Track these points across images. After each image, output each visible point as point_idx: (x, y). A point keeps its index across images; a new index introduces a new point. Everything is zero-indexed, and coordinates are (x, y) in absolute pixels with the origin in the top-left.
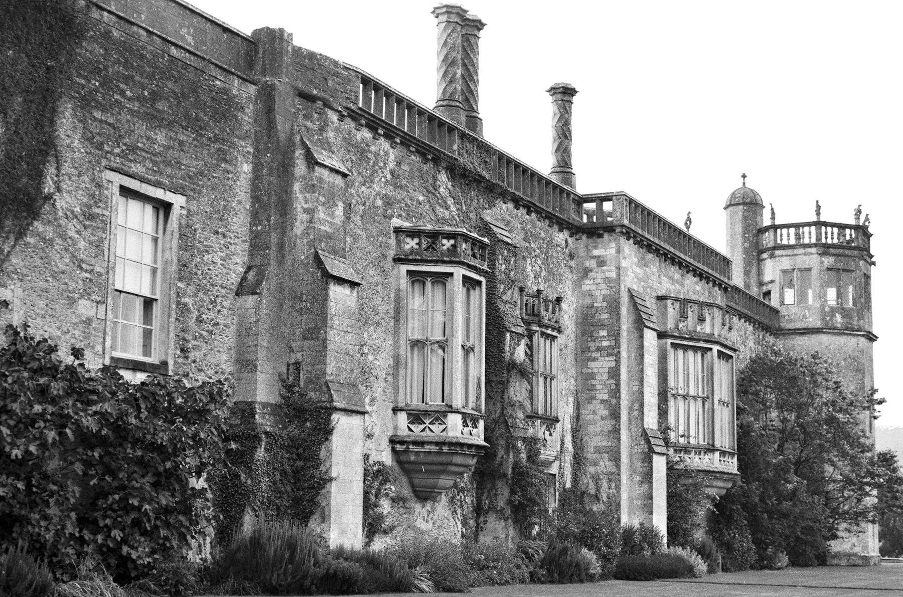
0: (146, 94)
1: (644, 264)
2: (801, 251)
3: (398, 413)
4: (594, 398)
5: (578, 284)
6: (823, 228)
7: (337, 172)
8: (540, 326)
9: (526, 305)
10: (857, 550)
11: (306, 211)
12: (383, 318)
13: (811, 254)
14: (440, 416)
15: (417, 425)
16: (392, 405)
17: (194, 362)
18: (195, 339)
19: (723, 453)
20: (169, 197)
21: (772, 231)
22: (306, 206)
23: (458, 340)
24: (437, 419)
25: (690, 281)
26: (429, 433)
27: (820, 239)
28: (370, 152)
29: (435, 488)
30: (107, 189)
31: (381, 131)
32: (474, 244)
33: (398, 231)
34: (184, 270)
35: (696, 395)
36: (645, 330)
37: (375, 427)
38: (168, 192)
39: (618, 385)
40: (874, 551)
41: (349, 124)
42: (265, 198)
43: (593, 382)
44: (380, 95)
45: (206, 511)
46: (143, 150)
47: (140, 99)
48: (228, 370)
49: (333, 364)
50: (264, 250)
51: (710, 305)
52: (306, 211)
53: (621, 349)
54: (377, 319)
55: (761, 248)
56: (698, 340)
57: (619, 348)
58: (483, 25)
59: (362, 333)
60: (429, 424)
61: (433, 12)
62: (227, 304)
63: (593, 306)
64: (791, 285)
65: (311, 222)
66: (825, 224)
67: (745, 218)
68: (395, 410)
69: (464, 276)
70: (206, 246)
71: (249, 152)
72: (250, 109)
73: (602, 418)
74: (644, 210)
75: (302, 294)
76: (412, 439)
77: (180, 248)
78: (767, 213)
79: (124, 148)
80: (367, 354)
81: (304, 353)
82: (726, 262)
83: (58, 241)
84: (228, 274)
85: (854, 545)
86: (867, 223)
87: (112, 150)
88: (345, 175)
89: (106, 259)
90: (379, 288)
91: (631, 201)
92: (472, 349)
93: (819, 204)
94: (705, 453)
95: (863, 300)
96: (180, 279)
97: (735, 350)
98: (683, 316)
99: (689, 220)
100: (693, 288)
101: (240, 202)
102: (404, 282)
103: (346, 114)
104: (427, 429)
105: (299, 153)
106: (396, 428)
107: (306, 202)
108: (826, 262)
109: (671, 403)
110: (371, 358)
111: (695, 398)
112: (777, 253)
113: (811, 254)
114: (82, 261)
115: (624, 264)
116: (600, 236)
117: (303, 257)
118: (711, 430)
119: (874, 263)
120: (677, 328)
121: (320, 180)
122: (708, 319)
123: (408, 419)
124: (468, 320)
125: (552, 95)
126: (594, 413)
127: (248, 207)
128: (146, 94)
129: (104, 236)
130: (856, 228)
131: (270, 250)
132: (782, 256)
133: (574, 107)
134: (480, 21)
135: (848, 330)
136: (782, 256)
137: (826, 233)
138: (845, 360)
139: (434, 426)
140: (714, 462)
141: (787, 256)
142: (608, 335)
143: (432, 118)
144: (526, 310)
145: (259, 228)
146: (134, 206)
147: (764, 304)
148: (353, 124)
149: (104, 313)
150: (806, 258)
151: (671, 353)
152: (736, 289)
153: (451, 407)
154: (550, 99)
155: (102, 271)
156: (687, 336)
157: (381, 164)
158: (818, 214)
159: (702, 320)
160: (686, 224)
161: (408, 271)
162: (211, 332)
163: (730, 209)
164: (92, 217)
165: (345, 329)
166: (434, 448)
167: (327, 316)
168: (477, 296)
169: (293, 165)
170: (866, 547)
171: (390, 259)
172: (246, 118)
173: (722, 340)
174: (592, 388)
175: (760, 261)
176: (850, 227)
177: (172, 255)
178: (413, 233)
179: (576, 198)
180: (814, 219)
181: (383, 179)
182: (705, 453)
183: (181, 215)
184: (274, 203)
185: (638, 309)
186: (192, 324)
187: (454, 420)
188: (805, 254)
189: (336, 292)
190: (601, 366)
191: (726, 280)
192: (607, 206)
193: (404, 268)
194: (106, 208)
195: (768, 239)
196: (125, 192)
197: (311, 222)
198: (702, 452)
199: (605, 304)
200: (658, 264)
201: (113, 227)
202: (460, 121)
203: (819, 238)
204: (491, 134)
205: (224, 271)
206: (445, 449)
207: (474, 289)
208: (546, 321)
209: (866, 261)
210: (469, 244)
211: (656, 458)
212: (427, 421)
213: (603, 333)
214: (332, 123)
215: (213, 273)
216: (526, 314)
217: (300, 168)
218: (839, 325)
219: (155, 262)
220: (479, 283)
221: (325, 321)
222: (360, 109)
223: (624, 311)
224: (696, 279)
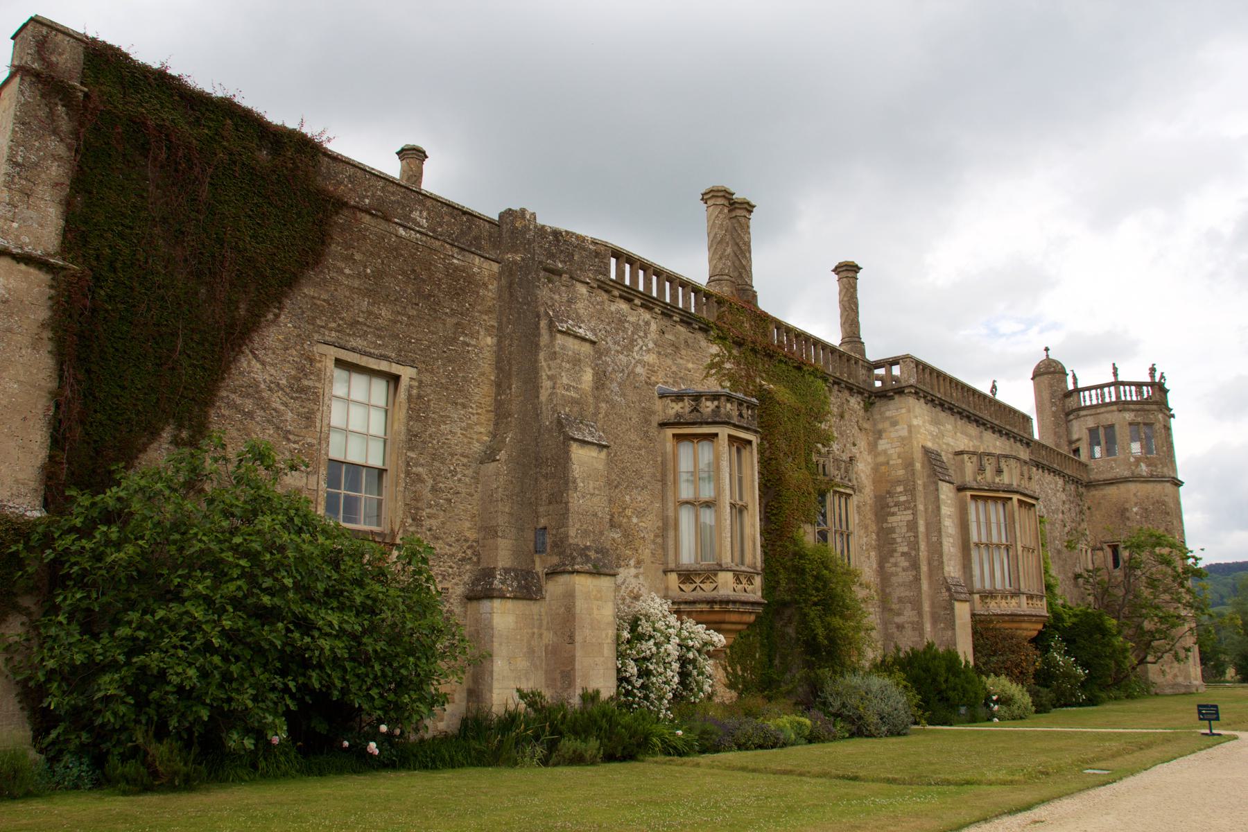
0: (369, 271)
1: (936, 422)
2: (1103, 410)
4: (895, 551)
5: (873, 447)
6: (1122, 388)
7: (583, 339)
10: (1180, 680)
13: (1113, 411)
14: (710, 574)
15: (688, 584)
16: (662, 567)
17: (430, 530)
18: (430, 506)
20: (395, 369)
22: (549, 373)
24: (708, 578)
25: (989, 436)
28: (628, 322)
30: (320, 361)
31: (637, 301)
32: (740, 404)
33: (662, 396)
34: (413, 439)
37: (642, 589)
38: (394, 364)
39: (916, 537)
40: (1196, 679)
43: (894, 536)
44: (634, 267)
45: (251, 691)
46: (365, 324)
47: (361, 276)
48: (472, 538)
49: (577, 526)
51: (1006, 457)
52: (550, 378)
56: (998, 491)
61: (702, 199)
62: (469, 472)
64: (1098, 444)
65: (554, 388)
66: (1124, 384)
67: (1051, 386)
69: (729, 436)
70: (442, 416)
71: (493, 326)
72: (493, 286)
73: (904, 570)
74: (932, 371)
77: (410, 418)
78: (1070, 380)
79: (341, 322)
82: (1026, 419)
83: (260, 413)
84: (470, 443)
85: (1175, 676)
87: (327, 324)
88: (593, 343)
89: (318, 430)
90: (643, 452)
92: (746, 507)
94: (1012, 597)
96: (411, 449)
99: (994, 388)
100: (994, 444)
101: (483, 374)
102: (669, 445)
107: (550, 369)
109: (974, 554)
110: (635, 520)
111: (998, 546)
112: (1082, 413)
113: (1113, 411)
114: (289, 432)
116: (891, 398)
119: (1173, 416)
120: (975, 480)
121: (563, 348)
122: (1005, 469)
123: (679, 578)
124: (740, 480)
126: (896, 565)
127: (493, 378)
128: (369, 271)
129: (316, 407)
130: (1152, 384)
132: (1086, 416)
134: (857, 266)
136: (1086, 416)
138: (1153, 504)
140: (1021, 606)
146: (359, 381)
147: (1076, 461)
149: (315, 483)
151: (972, 507)
153: (721, 565)
154: (836, 277)
155: (314, 442)
157: (642, 334)
158: (1115, 374)
159: (999, 471)
160: (992, 391)
162: (449, 501)
163: (1037, 379)
164: (303, 390)
165: (592, 491)
166: (705, 607)
169: (539, 335)
170: (1187, 677)
171: (655, 424)
172: (490, 294)
173: (1021, 490)
174: (893, 541)
176: (1146, 384)
177: (400, 426)
178: (679, 397)
180: (1112, 379)
183: (411, 387)
186: (427, 494)
187: (726, 579)
188: (1108, 412)
189: (577, 452)
191: (1026, 435)
192: (896, 370)
193: (670, 432)
194: (319, 380)
195: (1071, 403)
196: (339, 363)
197: (554, 388)
199: (900, 461)
201: (326, 399)
202: (725, 290)
203: (1118, 397)
205: (466, 440)
206: (717, 607)
210: (736, 405)
211: (957, 605)
212: (698, 581)
213: (900, 489)
215: (454, 441)
217: (545, 338)
218: (1145, 474)
219: (385, 434)
221: (567, 483)
222: (612, 280)
223: (918, 466)
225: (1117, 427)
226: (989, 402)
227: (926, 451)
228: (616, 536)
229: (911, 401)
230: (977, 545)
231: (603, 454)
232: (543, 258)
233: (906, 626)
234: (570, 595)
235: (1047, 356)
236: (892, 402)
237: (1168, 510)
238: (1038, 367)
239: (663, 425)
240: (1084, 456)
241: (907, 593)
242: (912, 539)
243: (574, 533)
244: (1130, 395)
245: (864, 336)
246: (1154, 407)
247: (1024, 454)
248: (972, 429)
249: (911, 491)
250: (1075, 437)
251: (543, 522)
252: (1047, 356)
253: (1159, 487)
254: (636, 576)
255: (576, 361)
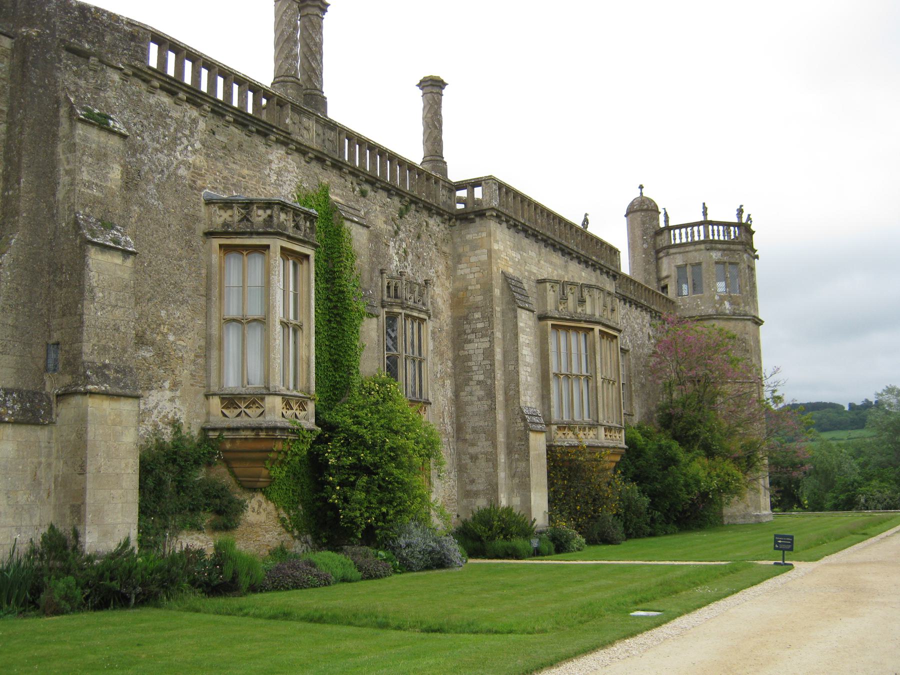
1: (518, 248)
2: (691, 248)
3: (211, 397)
6: (710, 227)
8: (403, 308)
9: (388, 287)
11: (68, 172)
12: (189, 296)
13: (701, 250)
15: (232, 410)
16: (204, 391)
19: (609, 429)
21: (666, 231)
22: (67, 168)
23: (278, 314)
24: (254, 402)
26: (246, 418)
27: (708, 236)
29: (259, 477)
33: (209, 202)
35: (579, 374)
36: (519, 310)
39: (492, 365)
41: (139, 86)
42: (16, 159)
43: (470, 364)
44: (197, 63)
50: (14, 217)
51: (589, 287)
52: (68, 172)
53: (495, 330)
54: (180, 297)
55: (658, 248)
56: (579, 321)
57: (493, 329)
58: (445, 84)
59: (158, 311)
60: (245, 408)
63: (467, 289)
66: (712, 223)
67: (644, 223)
68: (207, 396)
73: (479, 399)
75: (62, 265)
76: (225, 425)
78: (662, 218)
80: (167, 334)
81: (63, 331)
82: (614, 252)
86: (749, 222)
90: (184, 263)
91: (501, 186)
93: (706, 205)
94: (590, 428)
95: (748, 288)
97: (619, 331)
98: (564, 298)
99: (586, 221)
100: (579, 273)
103: (130, 73)
104: (243, 414)
105: (63, 111)
106: (208, 414)
108: (714, 257)
112: (672, 251)
113: (701, 250)
115: (496, 247)
116: (472, 221)
117: (64, 225)
118: (595, 407)
119: (757, 257)
121: (85, 139)
123: (222, 403)
125: (421, 89)
126: (471, 394)
130: (739, 225)
131: (19, 216)
132: (676, 253)
133: (444, 99)
134: (442, 81)
135: (734, 317)
136: (676, 253)
137: (713, 231)
139: (251, 409)
141: (680, 253)
142: (483, 317)
143: (420, 172)
144: (388, 292)
145: (10, 193)
148: (144, 86)
150: (695, 254)
152: (624, 277)
154: (421, 92)
156: (568, 318)
157: (187, 132)
158: (705, 213)
159: (582, 302)
161: (221, 246)
163: (630, 215)
165: (114, 302)
166: (250, 434)
167: (84, 287)
168: (305, 273)
169: (58, 124)
175: (658, 259)
178: (227, 204)
179: (447, 185)
181: (190, 148)
182: (590, 428)
184: (26, 164)
185: (512, 290)
188: (696, 250)
190: (476, 347)
192: (478, 193)
193: (216, 242)
198: (587, 429)
200: (537, 250)
202: (290, 94)
203: (707, 235)
204: (334, 113)
206: (263, 435)
207: (302, 263)
208: (410, 303)
209: (749, 254)
210: (291, 215)
211: (532, 436)
212: (243, 405)
213: (477, 315)
214: (114, 82)
216: (389, 296)
218: (728, 312)
220: (307, 257)
221: (82, 293)
223: (497, 292)
224: (582, 266)
225: (704, 266)
226: (580, 233)
227: (506, 277)
228: (148, 355)
229: (493, 225)
230: (556, 375)
231: (129, 262)
232: (66, 36)
233: (480, 456)
234: (82, 420)
235: (641, 193)
236: (473, 225)
237: (748, 348)
238: (632, 204)
239: (209, 234)
240: (671, 293)
241: (482, 423)
242: (488, 367)
243: (89, 350)
244: (718, 234)
245: (447, 155)
246: (740, 247)
247: (610, 286)
248: (557, 259)
249: (489, 318)
250: (664, 273)
251: (56, 336)
252: (641, 193)
253: (740, 325)
254: (172, 400)
255: (101, 156)
